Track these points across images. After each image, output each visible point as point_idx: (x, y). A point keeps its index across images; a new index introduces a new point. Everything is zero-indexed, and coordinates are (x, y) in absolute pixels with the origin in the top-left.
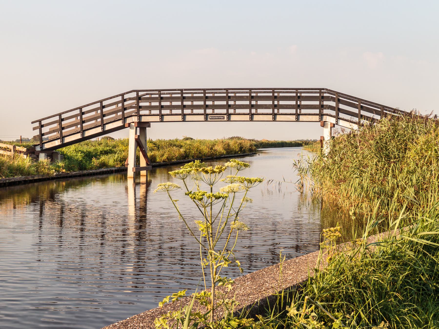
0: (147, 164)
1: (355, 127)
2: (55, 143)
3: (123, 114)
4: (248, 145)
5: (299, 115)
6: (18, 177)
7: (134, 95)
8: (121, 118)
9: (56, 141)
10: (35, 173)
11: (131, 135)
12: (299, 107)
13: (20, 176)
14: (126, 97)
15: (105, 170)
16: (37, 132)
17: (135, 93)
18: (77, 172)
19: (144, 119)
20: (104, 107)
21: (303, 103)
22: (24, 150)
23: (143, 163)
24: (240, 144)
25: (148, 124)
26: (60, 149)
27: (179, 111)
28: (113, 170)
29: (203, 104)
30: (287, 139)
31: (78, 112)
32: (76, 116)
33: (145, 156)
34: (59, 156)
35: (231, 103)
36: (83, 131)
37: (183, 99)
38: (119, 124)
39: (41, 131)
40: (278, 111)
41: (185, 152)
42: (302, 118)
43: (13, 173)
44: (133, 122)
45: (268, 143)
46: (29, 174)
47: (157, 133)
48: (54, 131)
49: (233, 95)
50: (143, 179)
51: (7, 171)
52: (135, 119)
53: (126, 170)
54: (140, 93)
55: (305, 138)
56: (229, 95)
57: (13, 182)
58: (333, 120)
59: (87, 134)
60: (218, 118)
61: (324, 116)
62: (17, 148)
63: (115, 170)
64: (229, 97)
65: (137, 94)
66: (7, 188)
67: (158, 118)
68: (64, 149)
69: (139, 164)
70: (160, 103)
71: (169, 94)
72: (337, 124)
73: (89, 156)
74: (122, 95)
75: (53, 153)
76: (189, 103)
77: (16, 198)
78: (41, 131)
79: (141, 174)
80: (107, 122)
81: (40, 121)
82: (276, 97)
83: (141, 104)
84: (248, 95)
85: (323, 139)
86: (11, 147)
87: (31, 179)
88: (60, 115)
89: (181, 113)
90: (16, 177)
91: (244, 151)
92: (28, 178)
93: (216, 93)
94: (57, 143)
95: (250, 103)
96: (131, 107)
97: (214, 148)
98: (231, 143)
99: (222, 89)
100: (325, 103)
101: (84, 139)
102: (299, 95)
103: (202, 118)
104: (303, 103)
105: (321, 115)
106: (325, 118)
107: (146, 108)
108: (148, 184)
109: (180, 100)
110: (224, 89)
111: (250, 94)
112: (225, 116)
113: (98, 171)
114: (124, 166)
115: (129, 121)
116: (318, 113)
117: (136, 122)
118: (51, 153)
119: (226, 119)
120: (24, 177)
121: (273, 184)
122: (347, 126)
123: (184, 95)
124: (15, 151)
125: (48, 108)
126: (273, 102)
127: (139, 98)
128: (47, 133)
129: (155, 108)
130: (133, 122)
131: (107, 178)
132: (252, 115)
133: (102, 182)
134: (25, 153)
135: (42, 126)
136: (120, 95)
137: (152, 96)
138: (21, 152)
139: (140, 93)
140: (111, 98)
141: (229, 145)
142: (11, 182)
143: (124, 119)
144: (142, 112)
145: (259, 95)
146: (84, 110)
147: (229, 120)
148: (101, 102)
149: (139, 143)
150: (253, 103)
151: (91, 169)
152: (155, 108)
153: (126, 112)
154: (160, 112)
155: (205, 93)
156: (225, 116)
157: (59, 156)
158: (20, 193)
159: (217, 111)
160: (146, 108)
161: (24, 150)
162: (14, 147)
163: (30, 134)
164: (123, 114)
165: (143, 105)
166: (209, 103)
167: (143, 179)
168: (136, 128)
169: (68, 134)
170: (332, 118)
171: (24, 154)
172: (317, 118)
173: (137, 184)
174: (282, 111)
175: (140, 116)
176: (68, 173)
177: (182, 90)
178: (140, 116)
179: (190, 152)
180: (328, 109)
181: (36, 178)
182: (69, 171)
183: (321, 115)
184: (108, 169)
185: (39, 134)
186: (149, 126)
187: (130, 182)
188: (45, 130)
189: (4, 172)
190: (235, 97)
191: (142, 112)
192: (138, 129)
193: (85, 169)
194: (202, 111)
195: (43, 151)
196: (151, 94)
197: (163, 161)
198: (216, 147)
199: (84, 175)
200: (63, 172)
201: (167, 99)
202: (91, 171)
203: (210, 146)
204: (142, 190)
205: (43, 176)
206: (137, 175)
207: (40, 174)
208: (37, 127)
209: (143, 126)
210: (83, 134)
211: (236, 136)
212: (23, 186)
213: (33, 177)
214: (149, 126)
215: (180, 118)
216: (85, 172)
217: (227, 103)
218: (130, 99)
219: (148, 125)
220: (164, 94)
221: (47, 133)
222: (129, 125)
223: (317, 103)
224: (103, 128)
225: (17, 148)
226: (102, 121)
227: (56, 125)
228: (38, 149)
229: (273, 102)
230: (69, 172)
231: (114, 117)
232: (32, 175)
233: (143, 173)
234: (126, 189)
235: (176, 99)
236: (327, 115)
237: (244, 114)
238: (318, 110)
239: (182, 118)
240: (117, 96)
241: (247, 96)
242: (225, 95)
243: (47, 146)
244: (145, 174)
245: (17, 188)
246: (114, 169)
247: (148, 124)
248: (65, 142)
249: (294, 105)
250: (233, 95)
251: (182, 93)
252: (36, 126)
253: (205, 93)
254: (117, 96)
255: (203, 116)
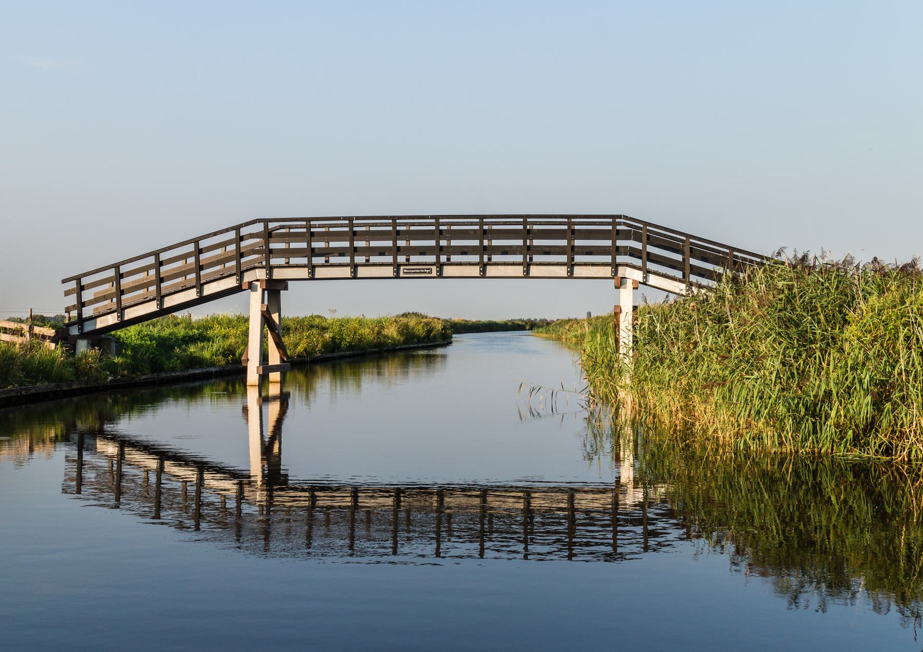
0: (282, 360)
4: (439, 327)
6: (42, 386)
7: (259, 228)
8: (234, 271)
9: (109, 316)
10: (73, 378)
11: (255, 303)
13: (47, 383)
14: (244, 231)
16: (72, 300)
19: (278, 274)
20: (200, 251)
22: (51, 332)
23: (275, 358)
25: (283, 284)
26: (113, 333)
28: (212, 372)
30: (500, 318)
32: (146, 269)
33: (280, 345)
35: (401, 243)
39: (79, 297)
40: (490, 259)
41: (333, 338)
42: (578, 271)
44: (258, 280)
45: (465, 325)
46: (61, 379)
48: (105, 298)
49: (404, 228)
50: (274, 390)
51: (21, 374)
52: (261, 274)
54: (271, 225)
55: (536, 316)
58: (638, 275)
59: (169, 302)
60: (420, 272)
62: (37, 330)
64: (398, 232)
65: (266, 227)
66: (23, 407)
67: (304, 273)
68: (120, 333)
70: (309, 244)
72: (644, 283)
74: (237, 228)
78: (79, 297)
79: (271, 380)
81: (78, 279)
83: (273, 246)
86: (26, 327)
87: (65, 388)
88: (117, 266)
89: (522, 260)
91: (419, 344)
94: (112, 319)
96: (254, 252)
98: (412, 322)
100: (578, 243)
101: (163, 312)
102: (528, 227)
104: (536, 242)
105: (615, 266)
106: (622, 271)
108: (284, 399)
109: (348, 238)
111: (481, 227)
112: (434, 268)
115: (248, 277)
116: (522, 260)
118: (99, 338)
119: (434, 274)
120: (53, 384)
121: (541, 396)
122: (668, 286)
124: (33, 335)
126: (481, 243)
127: (268, 235)
128: (92, 302)
130: (258, 280)
134: (54, 340)
136: (232, 228)
137: (292, 230)
138: (44, 337)
140: (215, 234)
143: (240, 274)
144: (274, 261)
147: (440, 276)
148: (196, 241)
149: (266, 319)
153: (243, 260)
159: (414, 259)
162: (31, 328)
163: (57, 305)
167: (274, 390)
168: (263, 290)
172: (607, 271)
173: (265, 400)
174: (496, 258)
175: (270, 269)
177: (350, 219)
179: (342, 339)
180: (625, 254)
181: (75, 387)
183: (615, 266)
185: (76, 303)
186: (286, 288)
187: (253, 395)
189: (15, 376)
191: (274, 261)
192: (266, 292)
193: (161, 369)
194: (389, 259)
195: (83, 335)
196: (290, 227)
197: (299, 356)
198: (385, 332)
199: (194, 378)
200: (123, 376)
203: (376, 329)
204: (274, 409)
206: (264, 379)
207: (80, 382)
208: (73, 289)
209: (274, 288)
210: (161, 303)
214: (286, 288)
215: (347, 272)
216: (163, 375)
217: (614, 243)
218: (252, 236)
221: (92, 302)
224: (200, 291)
225: (37, 330)
227: (107, 288)
231: (218, 271)
233: (275, 376)
234: (245, 410)
237: (513, 264)
238: (391, 257)
240: (227, 230)
241: (475, 231)
246: (213, 369)
247: (283, 284)
253: (395, 225)
254: (227, 230)
255: (349, 268)
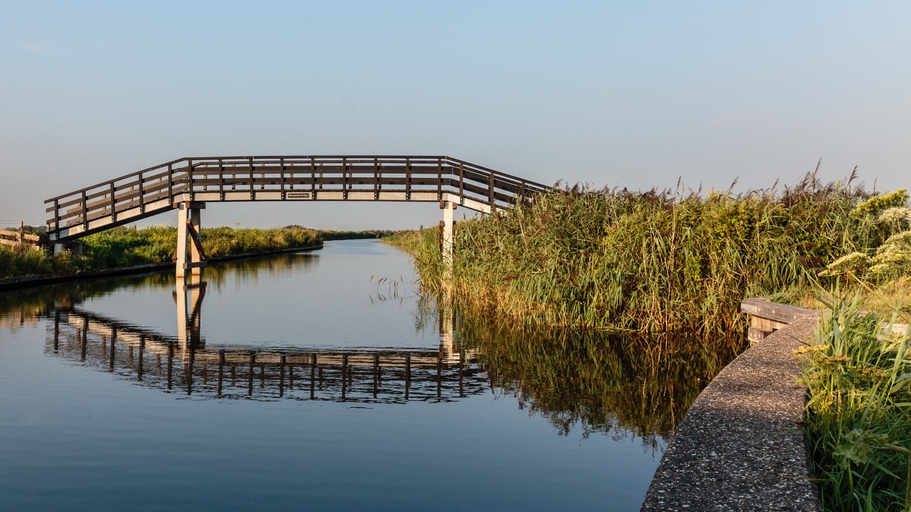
4: (314, 236)
6: (29, 276)
7: (185, 164)
9: (78, 227)
11: (182, 217)
12: (379, 181)
14: (174, 167)
16: (52, 215)
19: (199, 198)
21: (384, 175)
22: (37, 238)
24: (305, 234)
25: (202, 204)
27: (217, 188)
30: (357, 230)
33: (200, 249)
34: (81, 247)
36: (114, 214)
37: (223, 170)
38: (165, 203)
39: (57, 213)
40: (350, 187)
41: (238, 243)
46: (43, 271)
47: (216, 217)
48: (75, 214)
49: (289, 165)
50: (195, 280)
52: (186, 197)
54: (194, 162)
56: (443, 165)
58: (457, 199)
59: (120, 217)
60: (300, 197)
64: (285, 168)
65: (190, 163)
71: (231, 163)
72: (461, 205)
78: (57, 213)
81: (56, 200)
83: (194, 177)
84: (341, 164)
86: (18, 235)
91: (298, 248)
93: (296, 162)
94: (80, 229)
95: (313, 175)
96: (181, 181)
98: (294, 232)
99: (305, 157)
101: (116, 224)
104: (384, 175)
108: (202, 286)
110: (309, 157)
112: (310, 194)
113: (132, 268)
115: (177, 200)
118: (71, 243)
119: (310, 198)
121: (386, 285)
122: (478, 207)
124: (23, 240)
125: (69, 183)
126: (344, 175)
127: (192, 169)
128: (65, 217)
129: (213, 182)
133: (238, 267)
135: (58, 207)
136: (166, 165)
138: (31, 242)
139: (194, 162)
140: (154, 168)
141: (290, 235)
143: (171, 197)
145: (354, 164)
149: (190, 229)
150: (317, 175)
151: (123, 265)
152: (213, 182)
153: (173, 187)
154: (221, 188)
156: (310, 194)
157: (81, 247)
159: (296, 187)
161: (37, 238)
164: (171, 190)
165: (200, 177)
173: (189, 287)
174: (354, 187)
175: (193, 193)
177: (251, 158)
186: (204, 207)
187: (180, 284)
188: (63, 212)
190: (321, 167)
193: (115, 265)
195: (59, 241)
196: (207, 164)
198: (275, 239)
201: (229, 170)
204: (195, 294)
206: (188, 272)
207: (53, 275)
209: (196, 207)
214: (204, 207)
216: (116, 269)
218: (180, 170)
220: (257, 163)
221: (65, 217)
222: (179, 205)
224: (143, 210)
225: (27, 236)
229: (344, 175)
235: (212, 171)
236: (449, 192)
240: (162, 166)
242: (279, 165)
246: (152, 265)
247: (202, 204)
248: (90, 228)
251: (282, 162)
254: (162, 166)
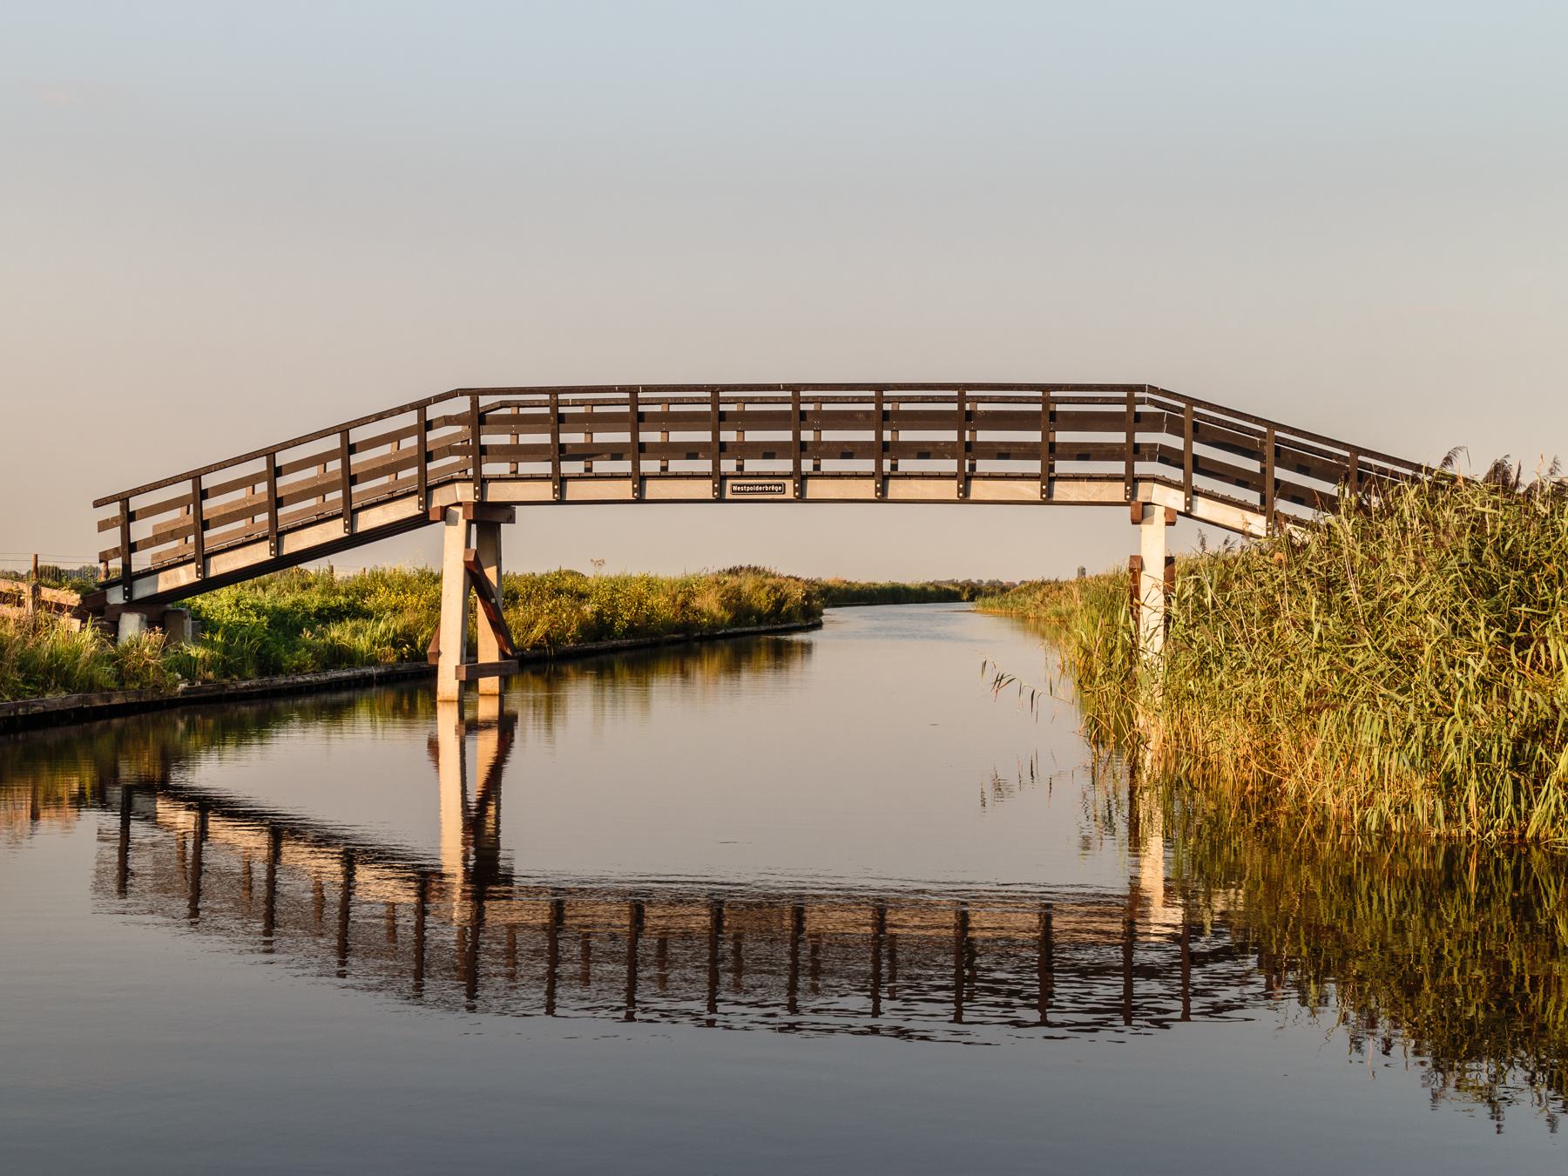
0: (503, 654)
1: (1258, 524)
2: (177, 577)
3: (423, 473)
5: (1052, 480)
6: (56, 698)
7: (462, 405)
9: (181, 570)
11: (451, 546)
13: (64, 694)
14: (433, 412)
15: (345, 674)
16: (113, 538)
17: (467, 399)
18: (254, 682)
19: (496, 493)
20: (352, 449)
22: (74, 599)
23: (489, 651)
25: (506, 510)
26: (188, 600)
27: (545, 468)
28: (371, 676)
29: (710, 440)
30: (912, 578)
31: (260, 465)
32: (250, 481)
34: (189, 623)
38: (409, 508)
39: (126, 533)
40: (894, 467)
41: (599, 614)
43: (36, 683)
44: (459, 504)
46: (90, 685)
47: (538, 546)
48: (173, 535)
49: (734, 408)
51: (15, 677)
52: (465, 492)
53: (432, 673)
54: (485, 401)
57: (39, 714)
58: (1176, 500)
59: (292, 544)
60: (762, 491)
61: (1141, 485)
63: (380, 676)
64: (722, 416)
65: (475, 404)
67: (545, 491)
69: (476, 655)
71: (583, 403)
72: (1187, 515)
73: (285, 624)
74: (421, 406)
75: (167, 612)
76: (578, 438)
77: (45, 779)
78: (126, 533)
80: (366, 502)
81: (124, 499)
82: (886, 415)
83: (486, 440)
85: (1137, 566)
87: (99, 703)
88: (196, 476)
90: (48, 696)
91: (760, 628)
92: (90, 701)
93: (751, 401)
94: (185, 576)
96: (452, 451)
97: (693, 604)
99: (776, 387)
101: (281, 562)
103: (705, 489)
104: (983, 436)
106: (1145, 492)
107: (503, 453)
108: (506, 725)
110: (787, 387)
111: (879, 406)
112: (789, 484)
113: (323, 678)
114: (425, 659)
115: (440, 498)
117: (468, 504)
118: (162, 611)
119: (789, 494)
120: (75, 697)
123: (642, 409)
124: (39, 603)
125: (155, 454)
127: (479, 419)
128: (148, 543)
129: (533, 452)
130: (459, 504)
131: (351, 704)
132: (883, 480)
133: (600, 675)
134: (80, 613)
135: (131, 517)
136: (412, 407)
137: (523, 411)
138: (60, 608)
139: (485, 401)
140: (380, 416)
142: (33, 715)
143: (426, 491)
144: (489, 469)
146: (282, 459)
147: (801, 498)
149: (474, 576)
151: (299, 670)
152: (533, 452)
155: (716, 401)
156: (789, 484)
157: (189, 623)
158: (60, 757)
159: (752, 465)
160: (503, 453)
164: (423, 473)
166: (650, 437)
167: (487, 709)
168: (469, 523)
169: (225, 545)
170: (1173, 491)
171: (75, 616)
174: (905, 465)
175: (482, 482)
176: (224, 686)
177: (633, 390)
178: (482, 482)
181: (116, 701)
182: (226, 676)
184: (358, 672)
185: (119, 544)
186: (511, 519)
187: (447, 721)
191: (489, 469)
192: (474, 527)
193: (278, 670)
195: (132, 605)
196: (519, 405)
197: (534, 647)
198: (697, 603)
200: (205, 681)
201: (579, 422)
202: (300, 679)
203: (680, 598)
204: (487, 744)
205: (139, 693)
209: (489, 519)
211: (745, 565)
212: (73, 731)
213: (109, 699)
214: (511, 519)
215: (625, 489)
216: (281, 680)
218: (448, 421)
219: (507, 513)
221: (148, 543)
223: (1035, 436)
224: (351, 524)
225: (47, 594)
226: (348, 498)
228: (116, 597)
230: (226, 681)
232: (103, 689)
234: (433, 746)
235: (533, 423)
239: (634, 490)
240: (402, 410)
243: (142, 590)
244: (497, 691)
245: (53, 736)
246: (373, 671)
247: (506, 510)
249: (1035, 444)
250: (811, 407)
252: (109, 516)
254: (402, 410)
